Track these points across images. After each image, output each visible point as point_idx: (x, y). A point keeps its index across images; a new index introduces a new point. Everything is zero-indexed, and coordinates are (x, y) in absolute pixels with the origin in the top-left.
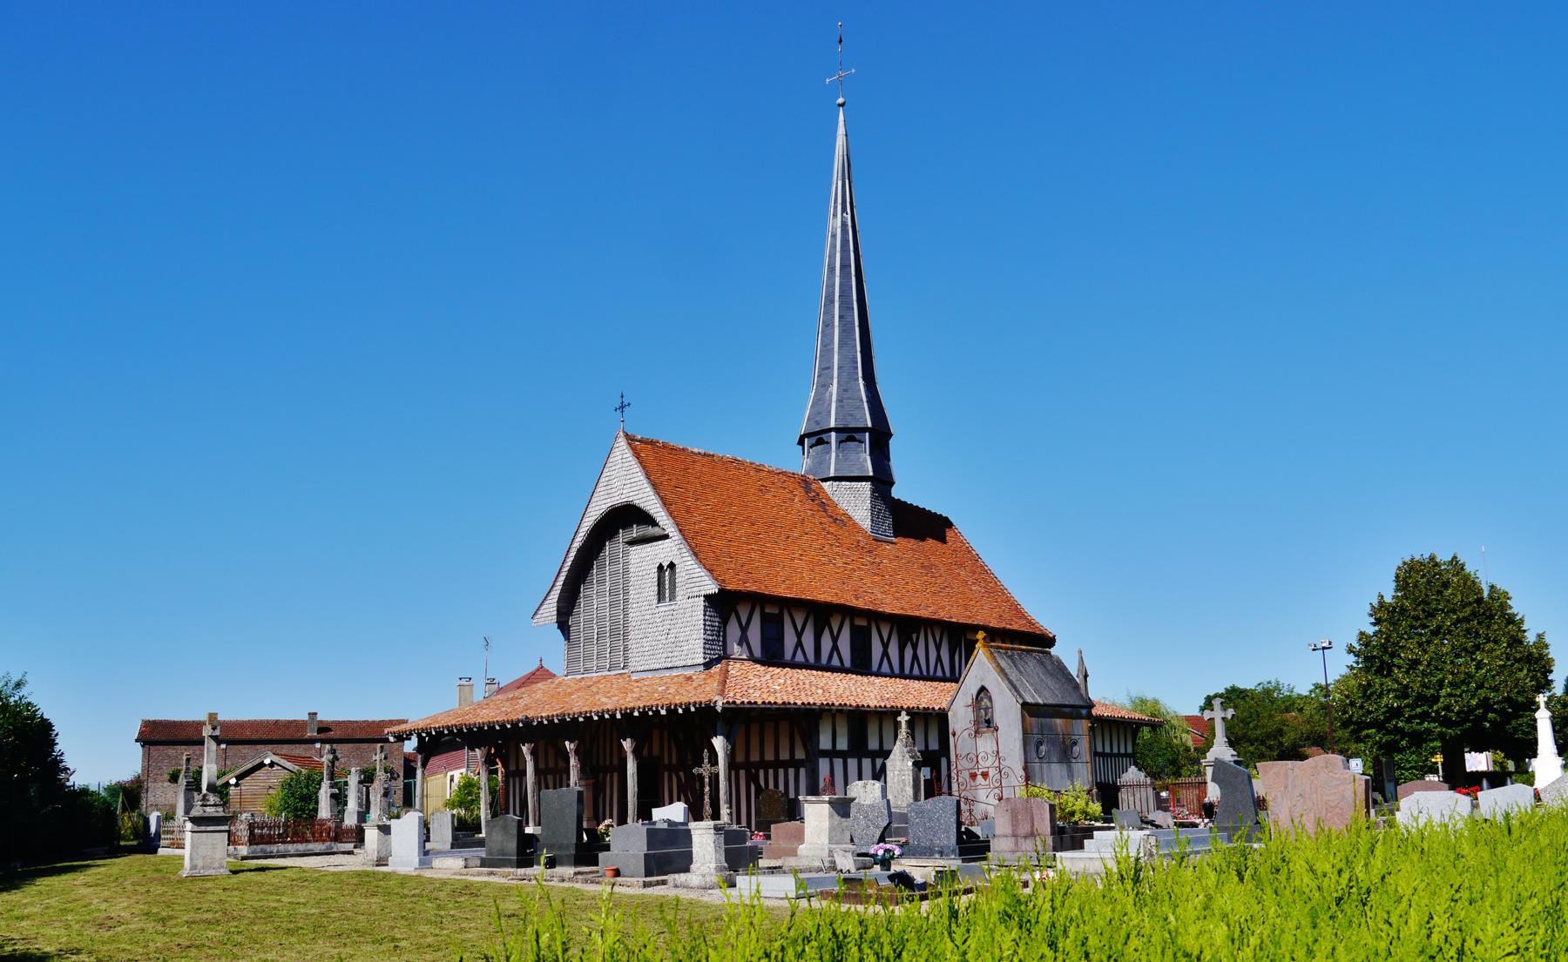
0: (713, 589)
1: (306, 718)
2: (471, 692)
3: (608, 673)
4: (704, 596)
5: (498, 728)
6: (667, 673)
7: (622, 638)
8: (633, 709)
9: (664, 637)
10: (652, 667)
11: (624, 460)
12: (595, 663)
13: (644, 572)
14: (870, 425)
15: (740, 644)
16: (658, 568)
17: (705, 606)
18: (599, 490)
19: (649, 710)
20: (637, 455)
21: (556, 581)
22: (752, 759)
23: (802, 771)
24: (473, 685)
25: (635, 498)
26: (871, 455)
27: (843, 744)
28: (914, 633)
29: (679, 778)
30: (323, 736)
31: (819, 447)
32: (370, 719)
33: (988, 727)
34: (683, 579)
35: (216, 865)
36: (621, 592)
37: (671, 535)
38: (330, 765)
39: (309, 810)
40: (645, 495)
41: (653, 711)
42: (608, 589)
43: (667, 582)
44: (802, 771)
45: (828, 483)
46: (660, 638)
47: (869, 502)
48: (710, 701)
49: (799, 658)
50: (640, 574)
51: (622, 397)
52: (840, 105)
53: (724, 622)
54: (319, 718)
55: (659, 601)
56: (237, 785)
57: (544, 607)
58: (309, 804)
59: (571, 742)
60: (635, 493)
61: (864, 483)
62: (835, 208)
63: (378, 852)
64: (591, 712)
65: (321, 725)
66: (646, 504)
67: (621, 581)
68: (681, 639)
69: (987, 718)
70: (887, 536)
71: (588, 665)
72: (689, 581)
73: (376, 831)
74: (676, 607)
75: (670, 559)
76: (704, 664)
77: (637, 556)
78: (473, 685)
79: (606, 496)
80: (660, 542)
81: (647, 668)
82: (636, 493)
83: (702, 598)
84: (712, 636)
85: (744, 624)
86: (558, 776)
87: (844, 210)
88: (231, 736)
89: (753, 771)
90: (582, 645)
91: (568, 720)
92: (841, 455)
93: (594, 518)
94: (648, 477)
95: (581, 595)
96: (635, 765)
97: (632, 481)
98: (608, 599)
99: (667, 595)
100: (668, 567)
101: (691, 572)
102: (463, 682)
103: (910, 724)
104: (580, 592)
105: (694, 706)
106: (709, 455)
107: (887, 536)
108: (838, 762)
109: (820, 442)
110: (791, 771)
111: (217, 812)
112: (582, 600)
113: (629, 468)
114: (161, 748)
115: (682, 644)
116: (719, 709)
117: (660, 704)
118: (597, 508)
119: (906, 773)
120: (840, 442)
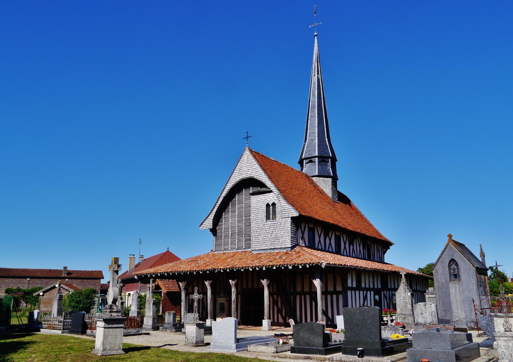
0: (296, 214)
1: (62, 269)
2: (134, 260)
3: (237, 251)
4: (291, 217)
5: (195, 273)
6: (272, 251)
7: (244, 236)
8: (273, 266)
9: (270, 235)
10: (263, 248)
11: (249, 159)
12: (230, 246)
13: (259, 207)
14: (331, 156)
15: (302, 240)
16: (266, 205)
17: (291, 222)
18: (236, 172)
19: (282, 266)
20: (255, 157)
21: (212, 210)
22: (329, 290)
23: (341, 297)
24: (135, 258)
25: (254, 175)
26: (331, 168)
27: (354, 285)
28: (355, 239)
30: (69, 276)
31: (310, 164)
32: (87, 270)
34: (280, 210)
35: (117, 348)
36: (244, 216)
37: (273, 191)
38: (121, 288)
39: (80, 307)
40: (260, 174)
41: (284, 267)
42: (237, 215)
43: (271, 211)
44: (341, 297)
45: (315, 178)
46: (268, 235)
47: (331, 186)
48: (319, 263)
50: (257, 208)
51: (247, 133)
52: (315, 35)
53: (297, 230)
54: (68, 269)
56: (43, 295)
57: (206, 221)
58: (80, 304)
59: (233, 280)
60: (254, 173)
61: (329, 179)
62: (315, 73)
63: (196, 339)
64: (288, 264)
65: (68, 272)
66: (260, 178)
67: (244, 211)
68: (279, 236)
69: (455, 274)
70: (336, 200)
71: (233, 246)
72: (283, 211)
73: (194, 327)
74: (276, 222)
75: (273, 201)
76: (291, 247)
77: (255, 200)
78: (135, 258)
79: (239, 175)
80: (268, 194)
81: (261, 248)
82: (255, 173)
83: (290, 218)
84: (293, 235)
85: (303, 231)
86: (303, 297)
87: (318, 74)
88: (32, 275)
90: (223, 238)
91: (235, 270)
92: (320, 167)
93: (233, 184)
94: (261, 166)
95: (223, 217)
96: (268, 292)
97: (253, 168)
98: (237, 219)
99: (271, 217)
100: (272, 204)
101: (284, 207)
102: (131, 256)
104: (222, 216)
105: (309, 265)
106: (277, 162)
107: (336, 200)
108: (353, 292)
109: (311, 161)
110: (335, 297)
111: (118, 316)
112: (223, 219)
113: (251, 163)
114: (3, 279)
115: (280, 238)
116: (323, 266)
117: (289, 263)
118: (234, 179)
119: (407, 298)
120: (319, 162)
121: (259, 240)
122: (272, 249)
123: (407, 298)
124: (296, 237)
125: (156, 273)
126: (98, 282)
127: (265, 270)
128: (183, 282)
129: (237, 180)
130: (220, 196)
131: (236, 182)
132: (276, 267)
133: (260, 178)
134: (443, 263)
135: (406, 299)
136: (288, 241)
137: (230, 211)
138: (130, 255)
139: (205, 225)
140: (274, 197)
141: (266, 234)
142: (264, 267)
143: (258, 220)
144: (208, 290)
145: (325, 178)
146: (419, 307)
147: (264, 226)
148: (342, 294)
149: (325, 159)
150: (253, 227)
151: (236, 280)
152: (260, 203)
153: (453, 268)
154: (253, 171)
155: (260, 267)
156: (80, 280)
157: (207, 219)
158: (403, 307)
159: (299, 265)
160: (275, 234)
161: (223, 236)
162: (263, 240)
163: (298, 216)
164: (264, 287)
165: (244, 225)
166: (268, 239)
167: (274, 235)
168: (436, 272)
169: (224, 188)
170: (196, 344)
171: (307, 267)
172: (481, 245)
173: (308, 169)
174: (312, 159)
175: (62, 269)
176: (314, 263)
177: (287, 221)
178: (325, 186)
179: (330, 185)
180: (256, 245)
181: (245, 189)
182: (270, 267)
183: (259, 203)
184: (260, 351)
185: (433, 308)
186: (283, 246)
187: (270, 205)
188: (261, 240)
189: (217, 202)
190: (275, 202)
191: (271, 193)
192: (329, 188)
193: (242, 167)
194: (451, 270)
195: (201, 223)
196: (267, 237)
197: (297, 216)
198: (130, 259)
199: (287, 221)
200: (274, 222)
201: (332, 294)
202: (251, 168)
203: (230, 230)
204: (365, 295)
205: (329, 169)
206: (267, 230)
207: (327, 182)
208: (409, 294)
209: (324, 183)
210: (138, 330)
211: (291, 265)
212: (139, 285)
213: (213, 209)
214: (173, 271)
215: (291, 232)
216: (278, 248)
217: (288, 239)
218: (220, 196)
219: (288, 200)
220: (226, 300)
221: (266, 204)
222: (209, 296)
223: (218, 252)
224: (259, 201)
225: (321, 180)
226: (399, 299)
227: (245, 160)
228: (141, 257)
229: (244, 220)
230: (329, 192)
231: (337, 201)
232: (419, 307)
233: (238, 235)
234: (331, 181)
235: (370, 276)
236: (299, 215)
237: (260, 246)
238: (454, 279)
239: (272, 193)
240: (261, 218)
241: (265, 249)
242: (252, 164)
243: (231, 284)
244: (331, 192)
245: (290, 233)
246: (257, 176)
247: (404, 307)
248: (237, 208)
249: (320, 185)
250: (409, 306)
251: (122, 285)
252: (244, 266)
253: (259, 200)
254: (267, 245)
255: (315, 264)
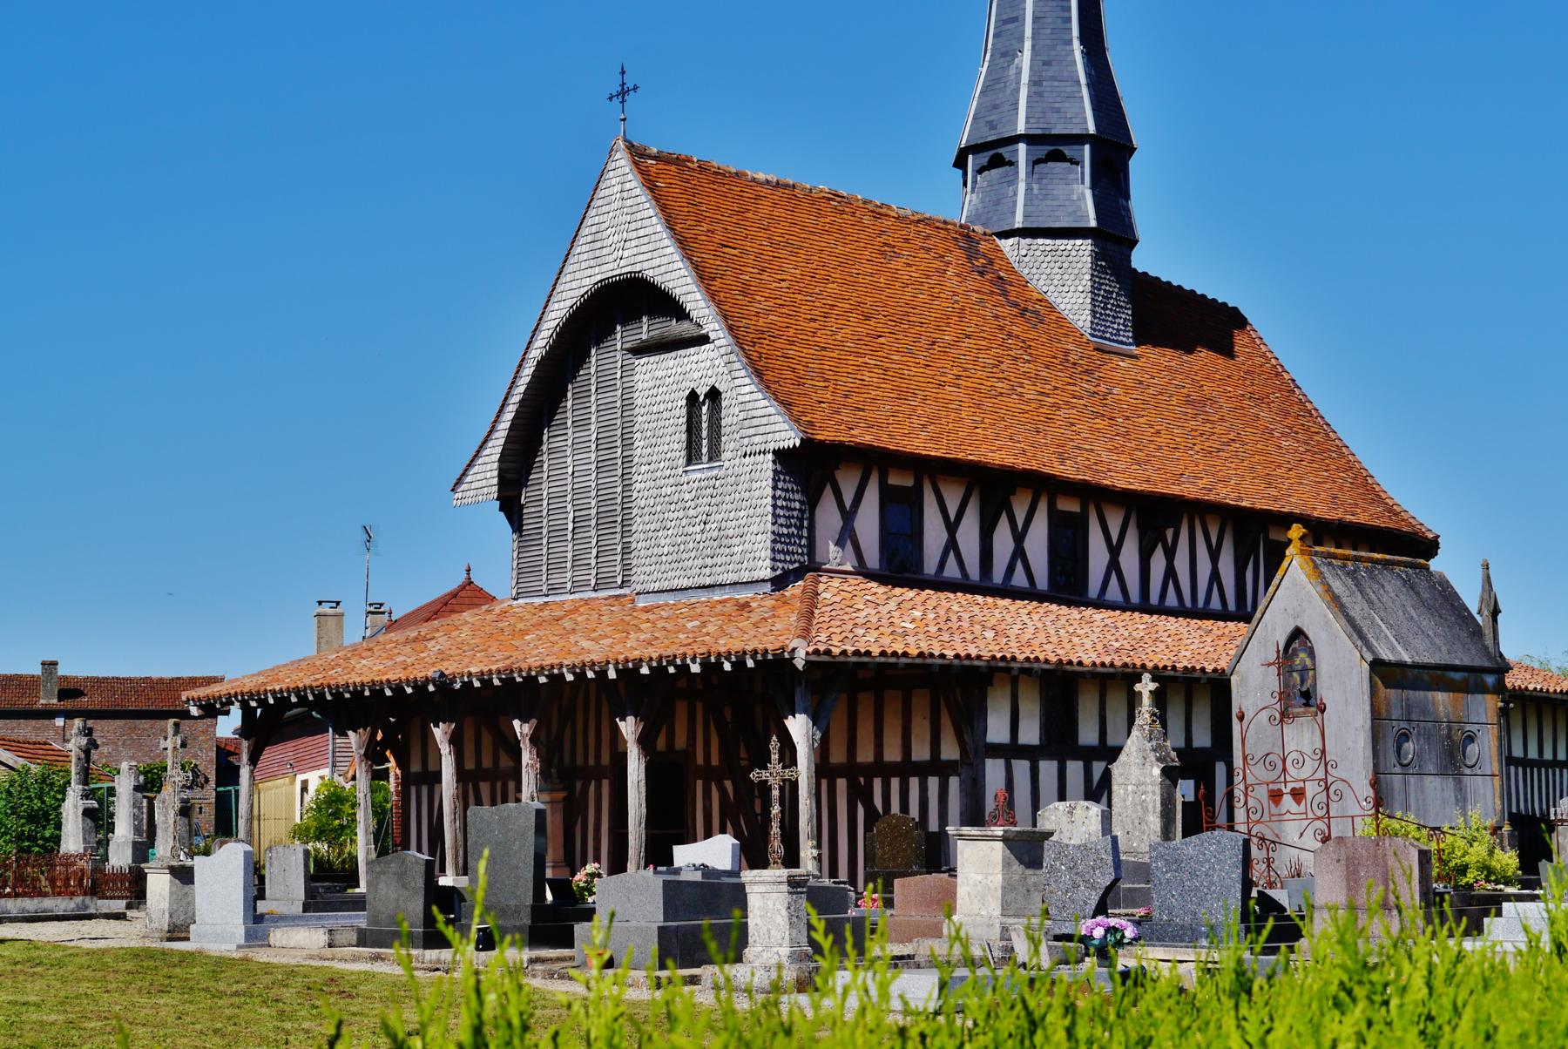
1: (37, 671)
2: (340, 627)
3: (594, 595)
4: (775, 452)
6: (703, 597)
7: (619, 529)
9: (698, 529)
10: (676, 583)
11: (625, 195)
12: (569, 575)
13: (662, 407)
15: (840, 543)
17: (775, 471)
19: (670, 663)
20: (650, 184)
22: (915, 757)
23: (954, 782)
24: (342, 615)
25: (646, 265)
27: (1030, 734)
29: (723, 792)
30: (68, 704)
33: (1307, 705)
37: (712, 336)
38: (83, 756)
39: (43, 838)
40: (665, 260)
41: (676, 667)
42: (594, 437)
45: (1011, 241)
46: (691, 529)
47: (1088, 277)
48: (783, 648)
49: (952, 570)
50: (655, 409)
51: (623, 73)
53: (812, 501)
54: (62, 671)
55: (689, 462)
57: (475, 469)
58: (44, 828)
59: (524, 720)
61: (1079, 242)
63: (171, 916)
65: (65, 686)
67: (619, 422)
68: (731, 532)
69: (1304, 689)
70: (1122, 343)
71: (556, 579)
74: (722, 473)
75: (711, 382)
78: (342, 615)
79: (592, 263)
80: (692, 350)
81: (666, 585)
82: (649, 256)
83: (770, 457)
84: (788, 527)
89: (862, 780)
90: (545, 541)
91: (519, 680)
92: (1035, 186)
93: (569, 303)
95: (544, 448)
97: (641, 233)
98: (593, 456)
99: (705, 450)
100: (706, 396)
102: (325, 609)
103: (1159, 698)
104: (541, 443)
106: (786, 186)
107: (1122, 343)
108: (1021, 767)
109: (997, 162)
113: (635, 209)
116: (799, 664)
117: (690, 653)
118: (574, 284)
119: (1150, 788)
121: (660, 550)
122: (704, 587)
123: (1150, 788)
124: (805, 534)
125: (258, 692)
126: (205, 732)
127: (615, 677)
128: (361, 730)
129: (586, 289)
130: (523, 360)
131: (583, 296)
132: (651, 668)
133: (667, 277)
134: (1265, 645)
135: (1145, 793)
136: (763, 554)
137: (569, 422)
138: (320, 603)
139: (473, 486)
140: (717, 362)
141: (684, 521)
142: (611, 666)
143: (657, 465)
144: (443, 759)
145: (1058, 242)
146: (1053, 818)
147: (679, 488)
148: (959, 775)
149: (1061, 148)
150: (641, 495)
151: (534, 722)
152: (665, 389)
153: (1300, 667)
154: (643, 249)
155: (597, 668)
156: (118, 722)
157: (480, 461)
158: (1133, 823)
159: (723, 660)
160: (715, 524)
161: (545, 531)
162: (672, 549)
163: (797, 445)
164: (629, 745)
165: (619, 483)
166: (691, 545)
167: (714, 526)
168: (1241, 680)
169: (538, 325)
170: (169, 932)
171: (589, 676)
172: (1486, 567)
173: (982, 201)
174: (1001, 150)
175: (37, 671)
176: (766, 651)
177: (759, 467)
178: (1058, 277)
179: (1084, 271)
180: (648, 569)
181: (623, 324)
182: (630, 665)
183: (661, 389)
184: (296, 945)
185: (1093, 821)
186: (745, 577)
187: (701, 399)
188: (666, 550)
189: (513, 383)
190: (717, 385)
191: (703, 347)
192: (1081, 288)
193: (604, 226)
194: (1295, 674)
195: (458, 477)
196: (688, 538)
197: (794, 445)
198: (319, 622)
199: (759, 467)
200: (715, 472)
201: (923, 770)
202: (634, 235)
203: (570, 506)
204: (1100, 781)
205: (1083, 195)
206: (688, 505)
207: (1070, 258)
208: (1157, 771)
209: (1052, 264)
210: (83, 901)
211: (698, 660)
212: (330, 742)
213: (498, 417)
214: (314, 684)
215: (775, 515)
216: (726, 585)
217: (761, 546)
218: (523, 360)
219: (769, 375)
220: (552, 802)
221: (687, 392)
222: (448, 784)
223: (528, 600)
224: (661, 382)
225: (1042, 248)
226: (1122, 791)
227: (613, 197)
228: (372, 613)
229: (619, 461)
230: (1076, 307)
231: (1130, 344)
232: (1053, 818)
233: (597, 525)
234: (1087, 253)
235: (914, 701)
236: (802, 439)
237: (665, 575)
238: (1302, 709)
239: (707, 346)
240: (668, 456)
241: (681, 589)
242: (639, 216)
243: (519, 735)
244: (1089, 307)
245: (770, 517)
246: (657, 271)
247: (1137, 822)
248: (593, 409)
249: (1036, 277)
250: (1152, 818)
251: (85, 742)
252: (548, 661)
253: (660, 374)
254: (689, 573)
255: (773, 655)
